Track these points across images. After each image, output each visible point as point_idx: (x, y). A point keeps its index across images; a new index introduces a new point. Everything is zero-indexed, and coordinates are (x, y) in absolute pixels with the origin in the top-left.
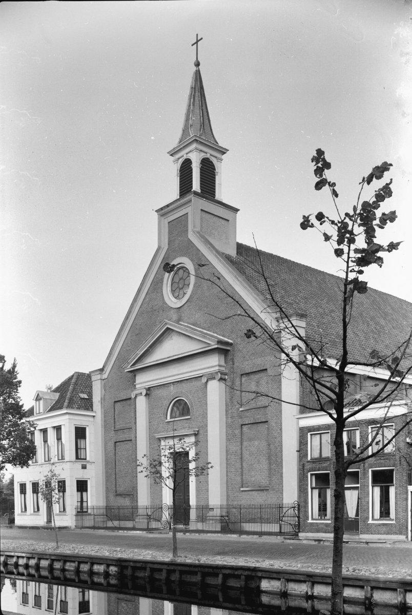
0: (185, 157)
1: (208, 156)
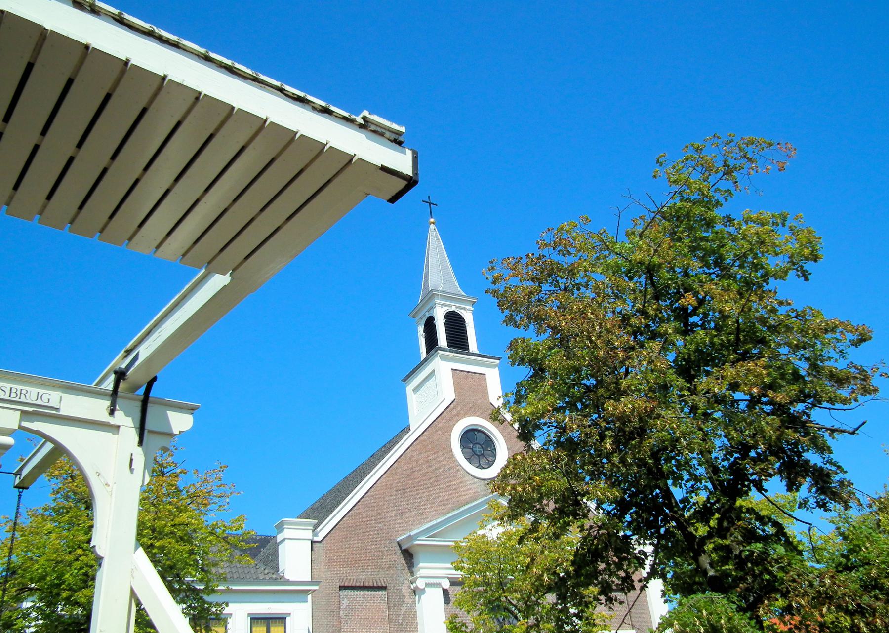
0: (427, 315)
1: (454, 309)
